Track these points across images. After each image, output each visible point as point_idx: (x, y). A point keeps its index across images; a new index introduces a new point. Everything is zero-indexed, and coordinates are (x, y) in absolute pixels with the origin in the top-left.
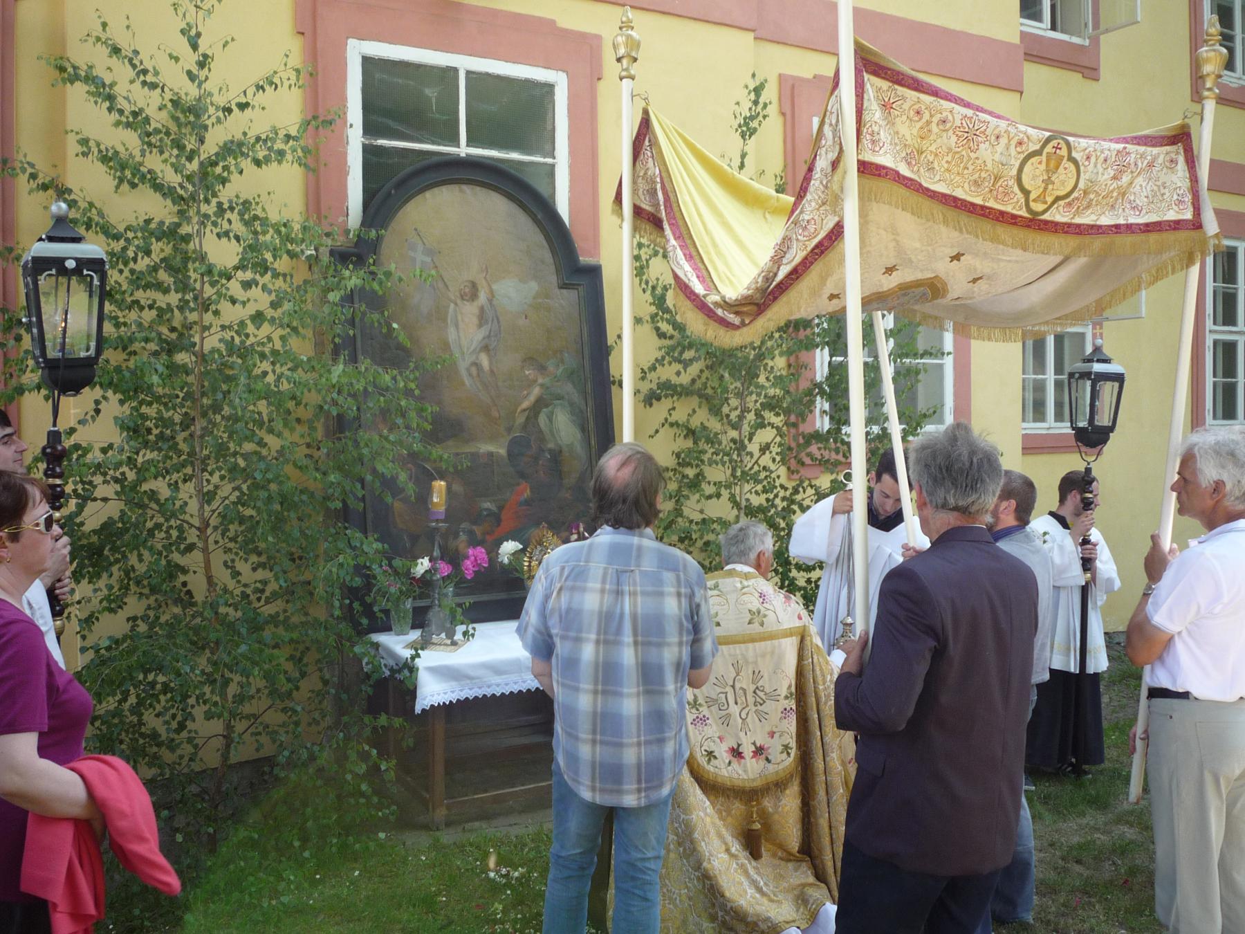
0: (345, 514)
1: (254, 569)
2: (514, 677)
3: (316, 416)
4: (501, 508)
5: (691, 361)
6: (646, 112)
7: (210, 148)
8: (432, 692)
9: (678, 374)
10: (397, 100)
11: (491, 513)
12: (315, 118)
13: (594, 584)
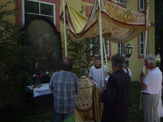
1: (8, 77)
2: (48, 92)
5: (74, 45)
6: (67, 4)
8: (36, 94)
9: (71, 47)
13: (60, 79)
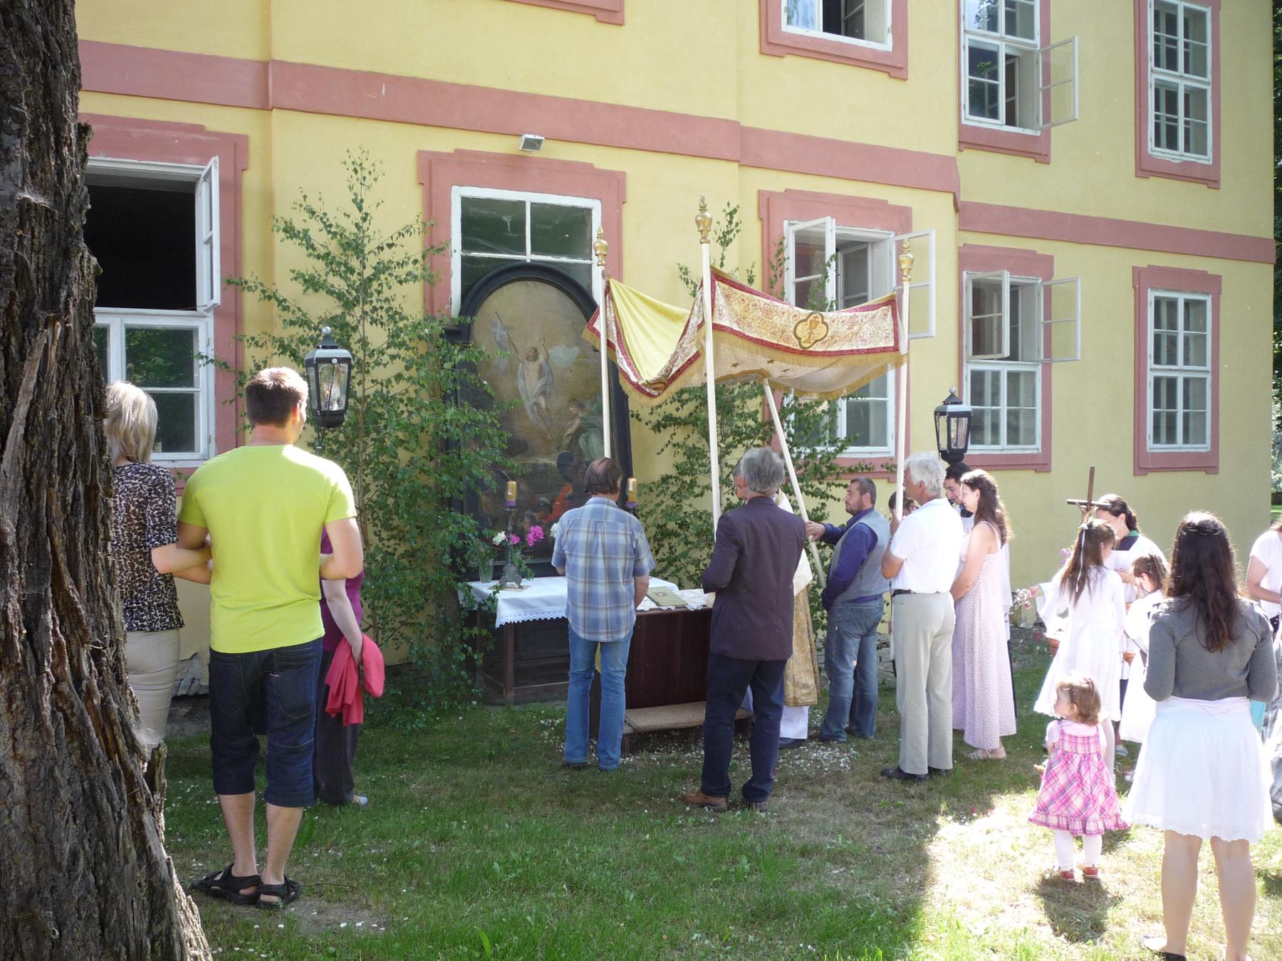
0: (449, 503)
4: (553, 501)
7: (368, 272)
8: (507, 614)
9: (678, 409)
10: (484, 225)
11: (545, 505)
12: (432, 247)
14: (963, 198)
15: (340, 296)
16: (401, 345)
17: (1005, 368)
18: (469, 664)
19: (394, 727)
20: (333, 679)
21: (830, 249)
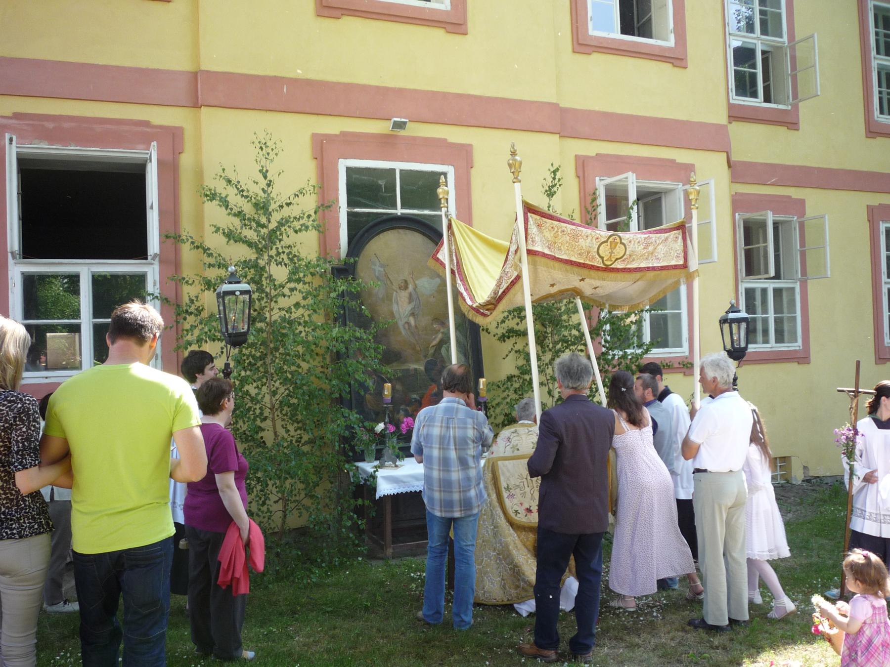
0: (340, 401)
1: (296, 431)
3: (326, 352)
4: (421, 398)
7: (273, 225)
8: (384, 488)
9: (518, 324)
10: (363, 188)
11: (416, 400)
12: (322, 205)
13: (438, 424)
14: (734, 158)
15: (250, 244)
16: (299, 281)
17: (771, 286)
18: (355, 527)
19: (293, 581)
20: (224, 556)
21: (632, 196)
